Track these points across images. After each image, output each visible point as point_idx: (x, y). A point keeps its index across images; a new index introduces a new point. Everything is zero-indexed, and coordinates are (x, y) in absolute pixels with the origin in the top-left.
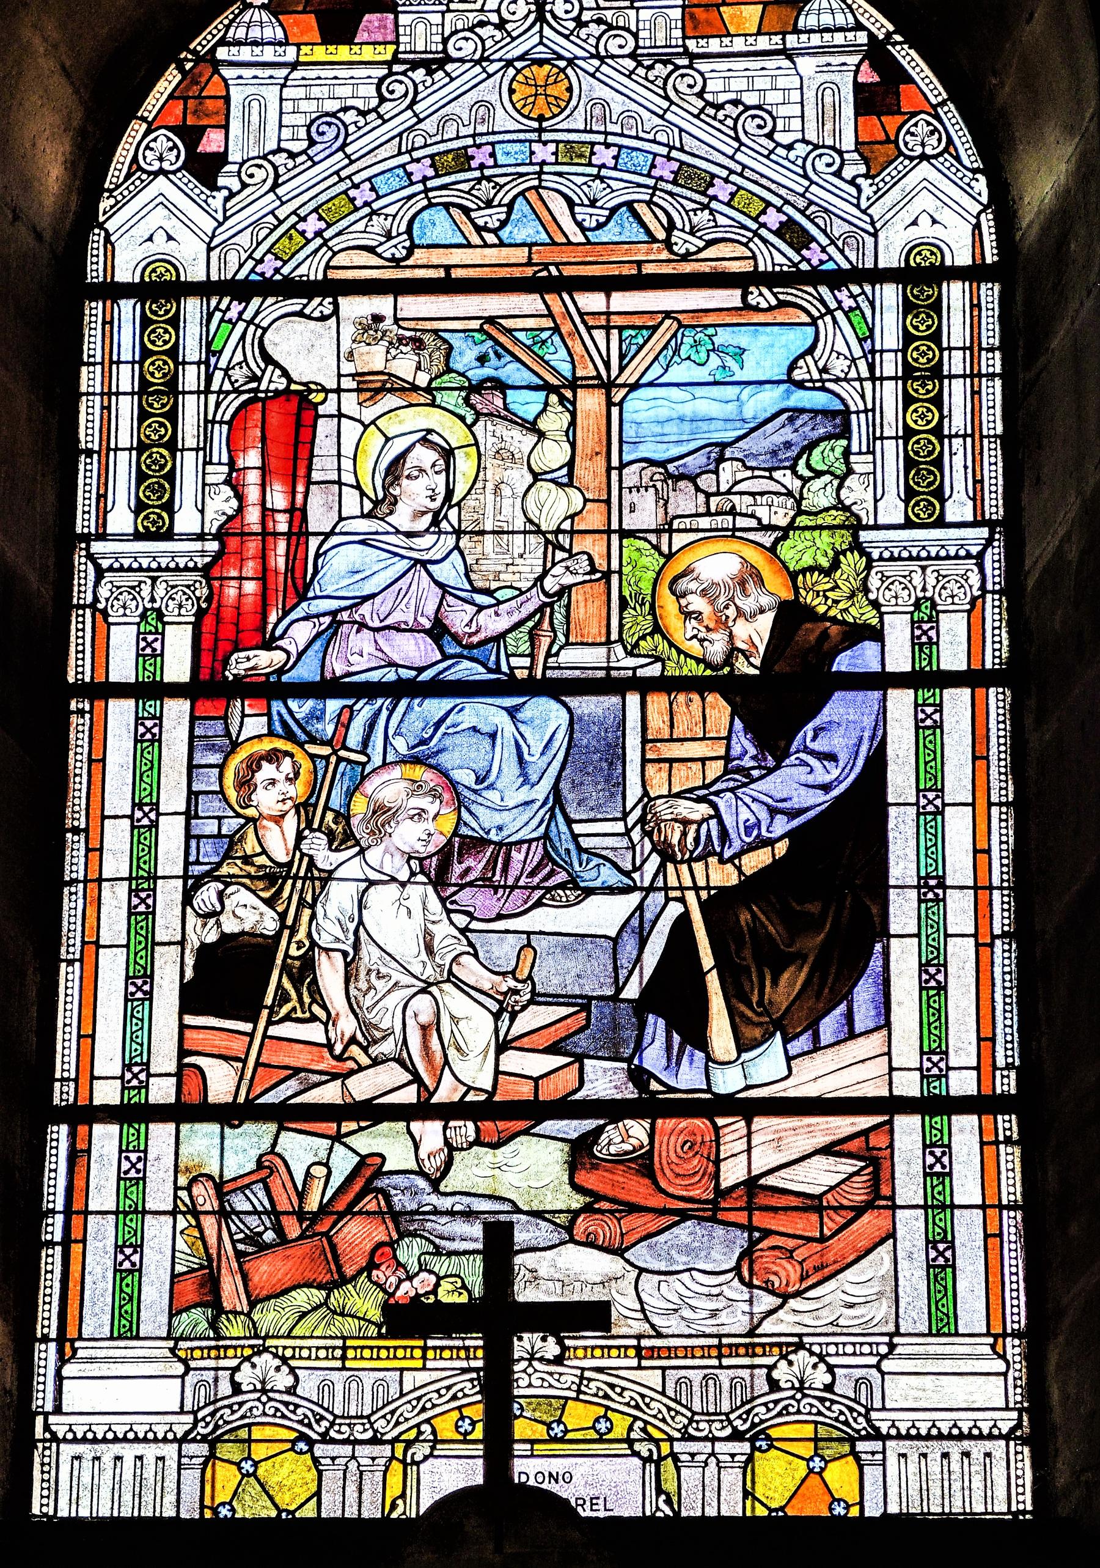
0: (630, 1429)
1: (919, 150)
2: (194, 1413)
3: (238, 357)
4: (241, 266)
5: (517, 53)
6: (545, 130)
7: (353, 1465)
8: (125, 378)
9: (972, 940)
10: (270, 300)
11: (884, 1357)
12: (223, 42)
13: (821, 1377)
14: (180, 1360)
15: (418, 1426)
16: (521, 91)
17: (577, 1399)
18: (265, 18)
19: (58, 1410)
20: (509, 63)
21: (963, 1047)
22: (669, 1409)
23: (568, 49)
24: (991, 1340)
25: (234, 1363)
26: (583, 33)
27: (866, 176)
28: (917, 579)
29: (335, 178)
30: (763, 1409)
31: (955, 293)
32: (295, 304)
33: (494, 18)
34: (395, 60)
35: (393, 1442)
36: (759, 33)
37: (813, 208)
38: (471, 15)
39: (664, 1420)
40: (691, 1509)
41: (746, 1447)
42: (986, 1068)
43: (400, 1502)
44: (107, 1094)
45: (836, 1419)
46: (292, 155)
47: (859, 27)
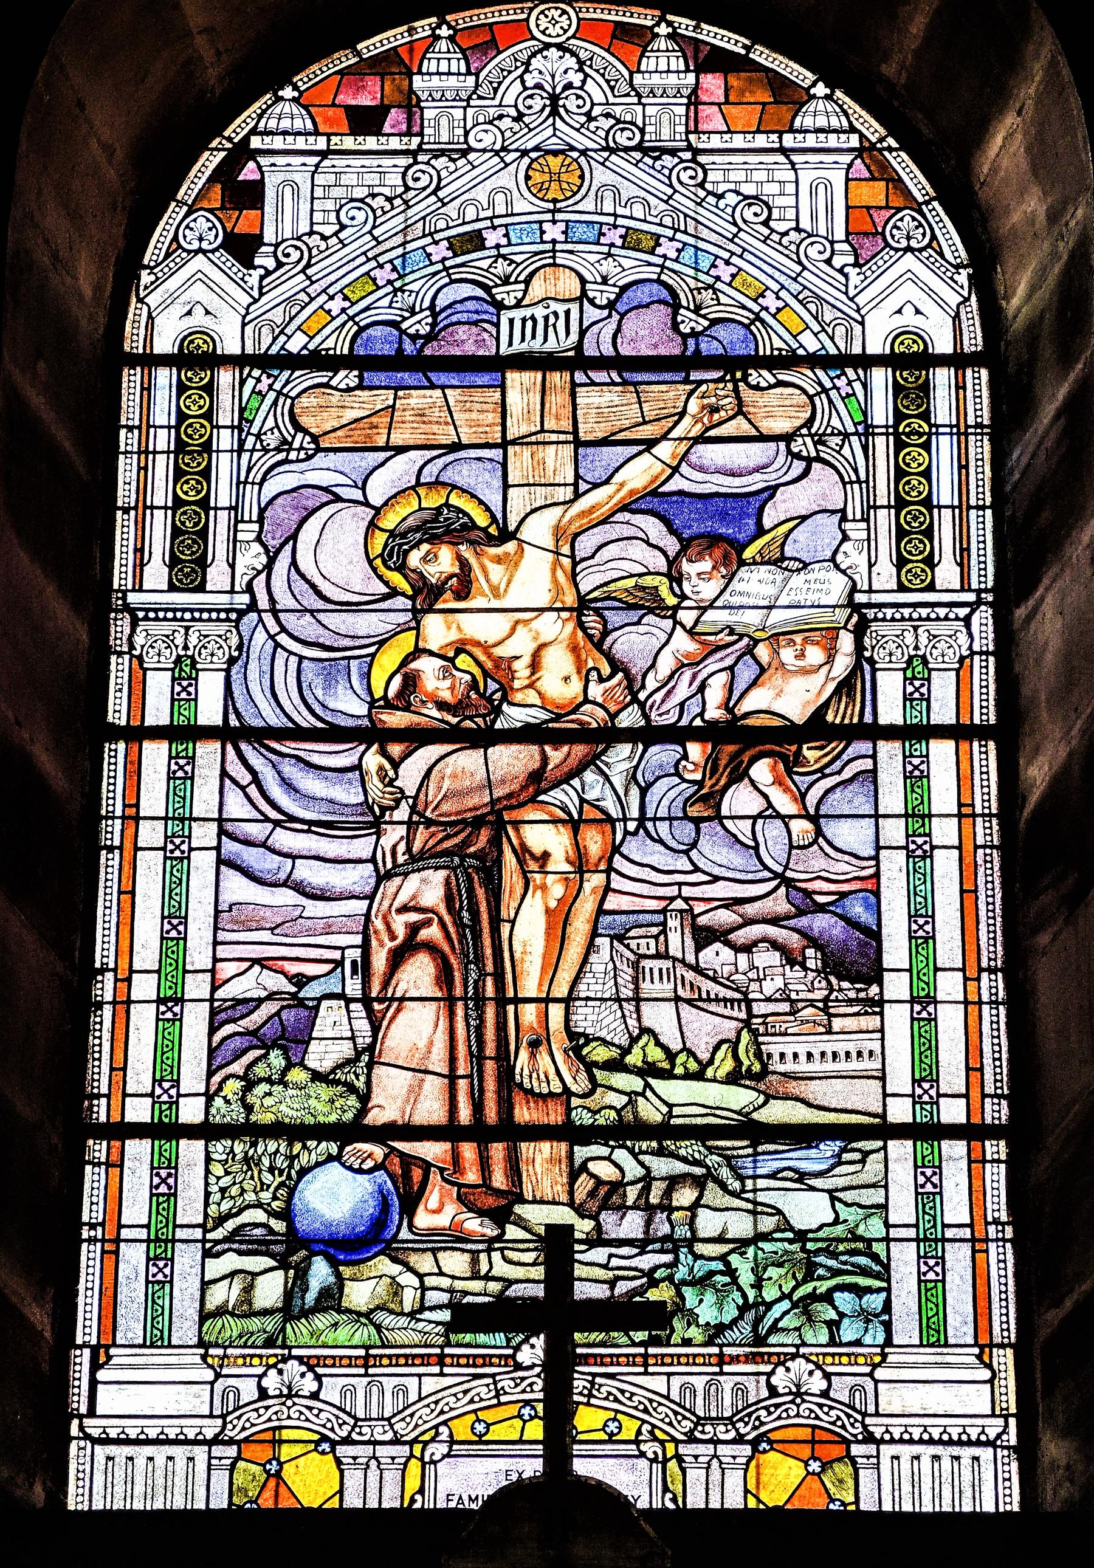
0: (639, 1432)
1: (904, 243)
2: (223, 1416)
3: (270, 423)
4: (275, 339)
5: (530, 145)
6: (559, 211)
7: (373, 1463)
8: (162, 440)
9: (959, 975)
10: (297, 373)
11: (875, 1366)
12: (254, 131)
13: (817, 1383)
14: (211, 1367)
15: (436, 1427)
16: (537, 177)
17: (588, 1404)
18: (295, 111)
19: (92, 1413)
20: (525, 153)
21: (952, 1077)
22: (676, 1413)
23: (581, 141)
24: (976, 1351)
25: (260, 1370)
26: (593, 126)
27: (856, 264)
28: (909, 638)
29: (363, 259)
30: (763, 1413)
31: (942, 377)
32: (321, 377)
33: (513, 112)
34: (420, 149)
35: (411, 1443)
36: (758, 131)
37: (806, 293)
38: (492, 111)
39: (670, 1424)
40: (695, 1500)
41: (747, 1450)
42: (975, 1094)
43: (418, 1497)
44: (138, 1112)
45: (833, 1423)
46: (324, 238)
47: (853, 130)
